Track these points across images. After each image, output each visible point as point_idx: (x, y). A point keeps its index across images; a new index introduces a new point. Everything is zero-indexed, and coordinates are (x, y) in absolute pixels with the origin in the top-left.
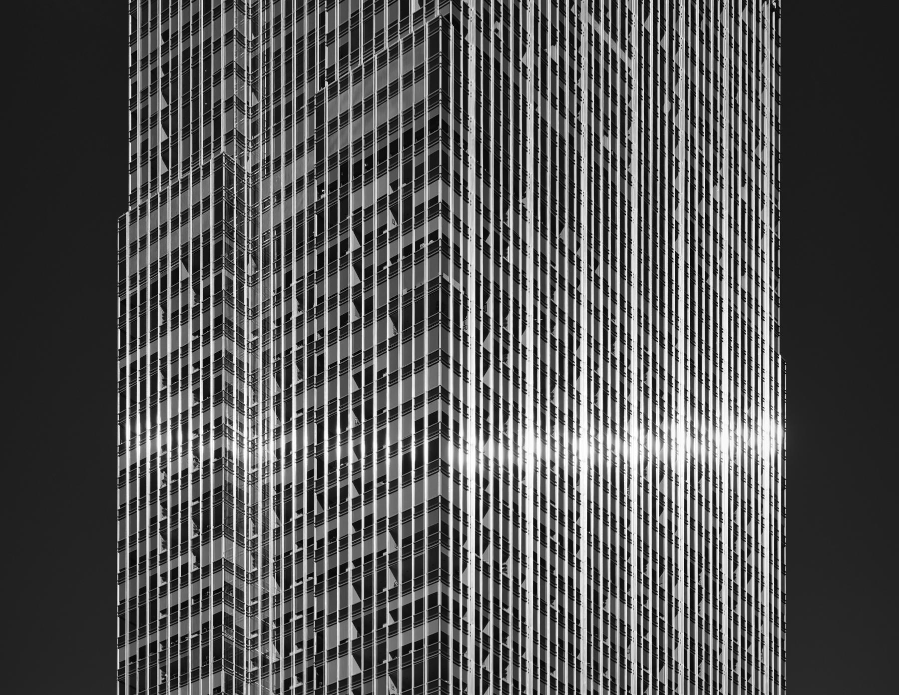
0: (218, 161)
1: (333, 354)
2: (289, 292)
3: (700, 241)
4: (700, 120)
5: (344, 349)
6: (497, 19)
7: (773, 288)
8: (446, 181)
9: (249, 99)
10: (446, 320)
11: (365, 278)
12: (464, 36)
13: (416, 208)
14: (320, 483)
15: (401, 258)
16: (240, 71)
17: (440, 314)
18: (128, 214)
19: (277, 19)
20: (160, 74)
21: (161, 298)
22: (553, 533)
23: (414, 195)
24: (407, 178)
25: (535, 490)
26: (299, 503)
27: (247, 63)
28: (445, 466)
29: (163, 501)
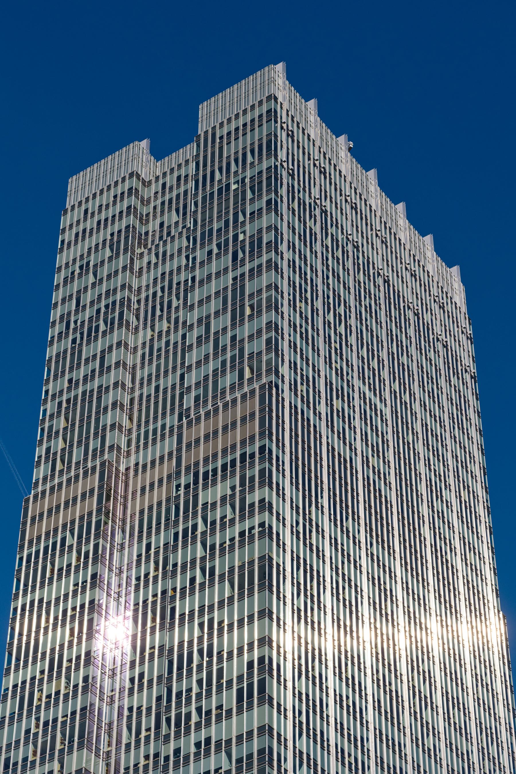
0: (103, 464)
1: (183, 606)
2: (148, 557)
3: (439, 528)
4: (433, 447)
5: (192, 603)
6: (302, 384)
7: (491, 562)
8: (271, 487)
9: (125, 422)
10: (271, 586)
11: (210, 551)
12: (282, 394)
13: (249, 505)
14: (168, 708)
15: (237, 539)
16: (122, 405)
17: (267, 582)
18: (32, 496)
19: (150, 375)
20: (64, 405)
21: (51, 557)
22: (350, 755)
23: (247, 496)
24: (242, 484)
25: (336, 719)
26: (148, 722)
27: (126, 401)
28: (271, 699)
29: (37, 716)
